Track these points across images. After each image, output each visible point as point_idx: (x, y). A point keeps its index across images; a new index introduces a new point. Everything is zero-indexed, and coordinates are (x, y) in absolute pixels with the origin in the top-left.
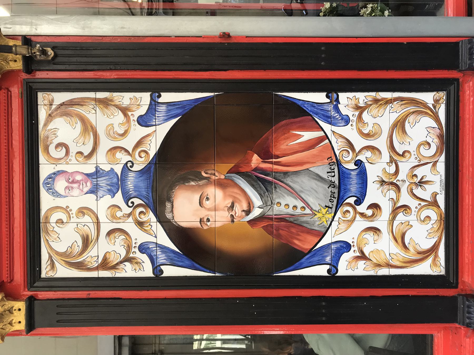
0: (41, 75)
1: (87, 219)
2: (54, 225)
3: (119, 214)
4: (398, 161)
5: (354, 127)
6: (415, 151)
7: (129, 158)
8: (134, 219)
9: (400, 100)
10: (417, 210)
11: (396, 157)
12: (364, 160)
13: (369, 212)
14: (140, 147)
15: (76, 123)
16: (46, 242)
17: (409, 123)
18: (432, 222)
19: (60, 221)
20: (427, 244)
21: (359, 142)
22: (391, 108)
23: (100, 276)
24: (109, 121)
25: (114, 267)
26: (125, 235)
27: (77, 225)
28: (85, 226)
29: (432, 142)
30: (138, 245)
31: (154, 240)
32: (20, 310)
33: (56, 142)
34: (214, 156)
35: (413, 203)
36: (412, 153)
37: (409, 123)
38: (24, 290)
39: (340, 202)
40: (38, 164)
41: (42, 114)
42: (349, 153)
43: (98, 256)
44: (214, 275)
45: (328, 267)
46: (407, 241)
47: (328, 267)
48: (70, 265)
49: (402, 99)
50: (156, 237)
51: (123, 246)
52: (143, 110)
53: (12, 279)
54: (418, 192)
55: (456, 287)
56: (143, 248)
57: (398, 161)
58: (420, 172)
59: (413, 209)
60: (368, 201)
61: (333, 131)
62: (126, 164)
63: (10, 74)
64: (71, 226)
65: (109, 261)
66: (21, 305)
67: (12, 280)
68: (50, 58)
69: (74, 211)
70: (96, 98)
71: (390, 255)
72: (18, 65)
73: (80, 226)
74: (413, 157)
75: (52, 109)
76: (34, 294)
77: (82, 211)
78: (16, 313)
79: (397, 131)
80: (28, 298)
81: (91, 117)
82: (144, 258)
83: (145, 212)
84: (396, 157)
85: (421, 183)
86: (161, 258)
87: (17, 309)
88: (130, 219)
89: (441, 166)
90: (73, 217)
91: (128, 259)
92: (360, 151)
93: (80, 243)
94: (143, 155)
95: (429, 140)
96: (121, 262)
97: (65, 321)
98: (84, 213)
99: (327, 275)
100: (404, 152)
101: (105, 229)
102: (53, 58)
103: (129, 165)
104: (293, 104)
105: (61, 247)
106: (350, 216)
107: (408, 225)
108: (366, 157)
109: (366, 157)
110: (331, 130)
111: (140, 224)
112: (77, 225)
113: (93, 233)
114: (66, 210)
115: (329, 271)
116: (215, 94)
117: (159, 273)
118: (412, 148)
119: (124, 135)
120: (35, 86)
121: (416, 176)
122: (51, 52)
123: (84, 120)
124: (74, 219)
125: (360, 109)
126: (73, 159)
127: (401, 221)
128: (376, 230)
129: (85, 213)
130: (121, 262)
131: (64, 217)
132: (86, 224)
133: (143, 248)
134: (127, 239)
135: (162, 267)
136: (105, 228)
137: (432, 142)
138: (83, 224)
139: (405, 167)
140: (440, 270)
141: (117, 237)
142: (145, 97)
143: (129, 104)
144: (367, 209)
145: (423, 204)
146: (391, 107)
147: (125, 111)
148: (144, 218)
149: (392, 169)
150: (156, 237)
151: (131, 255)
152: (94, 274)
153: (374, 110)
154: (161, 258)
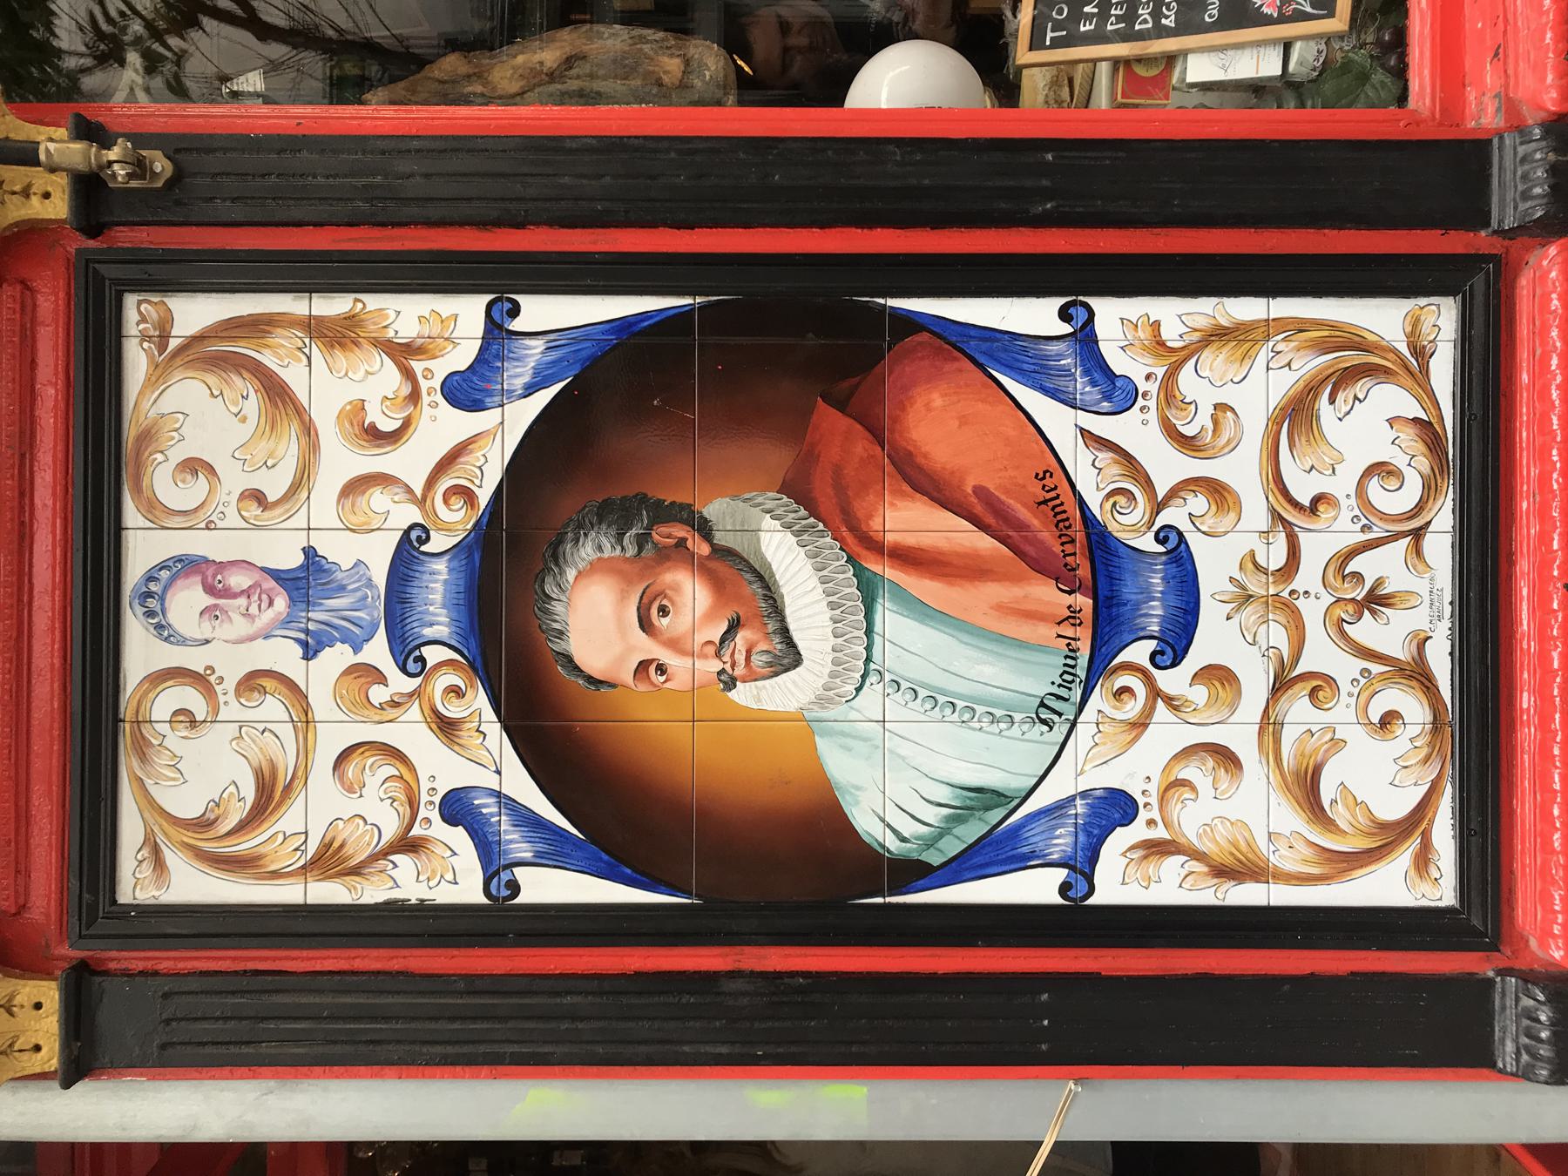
0: (127, 237)
1: (273, 708)
2: (164, 728)
3: (378, 694)
4: (1297, 529)
5: (1152, 415)
6: (1353, 495)
7: (413, 515)
8: (427, 711)
9: (1292, 328)
10: (1356, 691)
11: (1290, 515)
12: (1184, 525)
13: (1199, 694)
14: (452, 475)
15: (243, 397)
16: (135, 784)
17: (1180, 336)
18: (1413, 730)
19: (185, 717)
20: (1395, 805)
21: (1167, 466)
22: (1271, 354)
23: (313, 899)
24: (355, 392)
25: (356, 871)
26: (398, 764)
27: (241, 728)
28: (265, 734)
29: (1409, 465)
30: (437, 799)
31: (491, 782)
32: (38, 1006)
33: (177, 454)
34: (692, 450)
35: (1344, 668)
36: (1344, 502)
37: (1180, 336)
38: (61, 942)
39: (1100, 666)
40: (119, 528)
41: (137, 361)
42: (1130, 496)
43: (306, 833)
44: (690, 901)
45: (1061, 874)
46: (1327, 792)
47: (1061, 874)
48: (197, 855)
49: (1300, 326)
50: (499, 772)
51: (391, 801)
52: (462, 356)
53: (21, 901)
54: (1366, 630)
55: (1494, 948)
56: (456, 808)
57: (1297, 529)
58: (1367, 565)
59: (1345, 686)
60: (1197, 657)
61: (1082, 429)
62: (407, 532)
63: (31, 233)
64: (217, 738)
65: (351, 852)
66: (49, 993)
67: (23, 908)
68: (159, 184)
69: (230, 684)
70: (310, 316)
71: (1270, 837)
72: (58, 207)
73: (246, 733)
74: (1345, 515)
75: (170, 349)
76: (91, 958)
77: (253, 682)
78: (25, 1016)
79: (1303, 439)
80: (73, 968)
81: (293, 375)
82: (459, 837)
83: (463, 688)
84: (1290, 515)
85: (1376, 600)
86: (518, 845)
87: (28, 1004)
88: (414, 712)
89: (1440, 546)
90: (226, 703)
91: (408, 844)
92: (1173, 493)
93: (249, 792)
94: (458, 502)
95: (1400, 461)
96: (385, 853)
97: (222, 1050)
98: (264, 688)
99: (1059, 900)
100: (1318, 500)
101: (329, 743)
102: (172, 183)
103: (414, 535)
104: (911, 324)
105: (186, 802)
106: (1132, 709)
107: (1332, 739)
108: (1190, 514)
109: (1190, 514)
110: (1076, 425)
111: (446, 728)
112: (241, 728)
113: (287, 762)
114: (201, 680)
115: (1064, 889)
116: (699, 300)
117: (505, 893)
118: (1342, 485)
119: (394, 437)
120: (108, 271)
121: (1358, 577)
122: (161, 165)
123: (276, 392)
124: (232, 709)
125: (1176, 358)
126: (231, 511)
127: (1308, 727)
128: (1225, 757)
129: (267, 690)
130: (385, 853)
131: (197, 703)
132: (269, 726)
133: (456, 808)
134: (402, 778)
135: (519, 872)
136: (332, 738)
137: (1409, 465)
138: (261, 727)
139: (1318, 548)
140: (1442, 891)
141: (238, 744)
142: (469, 312)
143: (415, 336)
144: (1191, 686)
145: (1376, 668)
146: (1272, 351)
147: (403, 353)
148: (453, 710)
149: (1276, 556)
150: (499, 772)
151: (416, 831)
152: (288, 893)
153: (1214, 360)
154: (518, 845)
